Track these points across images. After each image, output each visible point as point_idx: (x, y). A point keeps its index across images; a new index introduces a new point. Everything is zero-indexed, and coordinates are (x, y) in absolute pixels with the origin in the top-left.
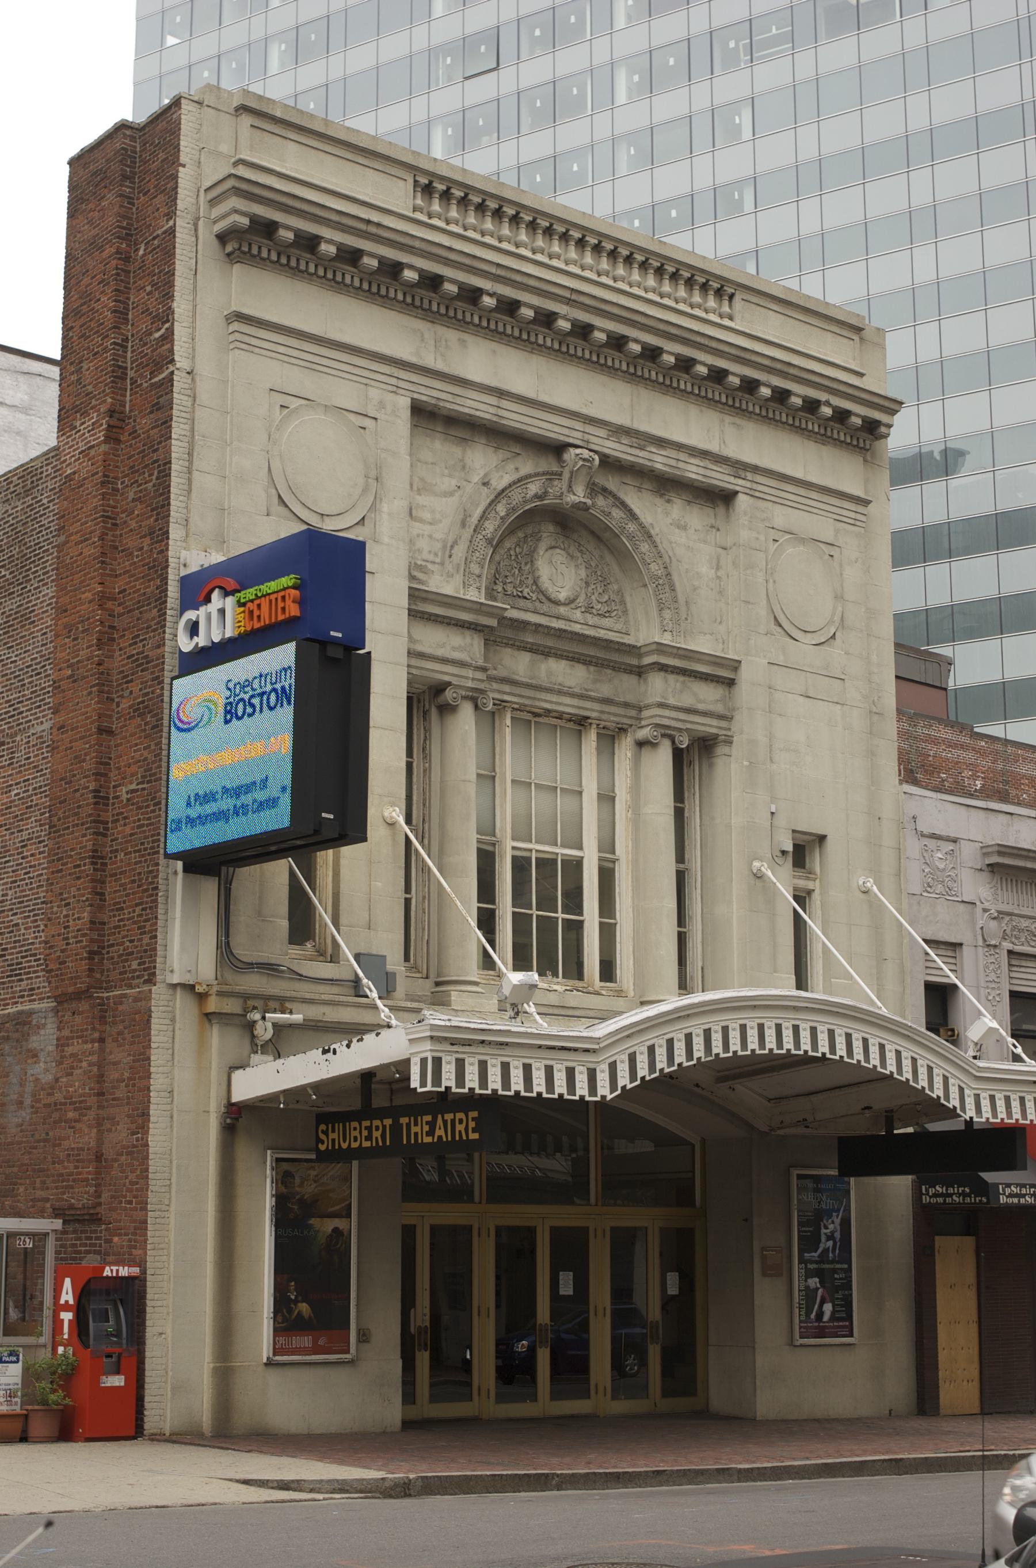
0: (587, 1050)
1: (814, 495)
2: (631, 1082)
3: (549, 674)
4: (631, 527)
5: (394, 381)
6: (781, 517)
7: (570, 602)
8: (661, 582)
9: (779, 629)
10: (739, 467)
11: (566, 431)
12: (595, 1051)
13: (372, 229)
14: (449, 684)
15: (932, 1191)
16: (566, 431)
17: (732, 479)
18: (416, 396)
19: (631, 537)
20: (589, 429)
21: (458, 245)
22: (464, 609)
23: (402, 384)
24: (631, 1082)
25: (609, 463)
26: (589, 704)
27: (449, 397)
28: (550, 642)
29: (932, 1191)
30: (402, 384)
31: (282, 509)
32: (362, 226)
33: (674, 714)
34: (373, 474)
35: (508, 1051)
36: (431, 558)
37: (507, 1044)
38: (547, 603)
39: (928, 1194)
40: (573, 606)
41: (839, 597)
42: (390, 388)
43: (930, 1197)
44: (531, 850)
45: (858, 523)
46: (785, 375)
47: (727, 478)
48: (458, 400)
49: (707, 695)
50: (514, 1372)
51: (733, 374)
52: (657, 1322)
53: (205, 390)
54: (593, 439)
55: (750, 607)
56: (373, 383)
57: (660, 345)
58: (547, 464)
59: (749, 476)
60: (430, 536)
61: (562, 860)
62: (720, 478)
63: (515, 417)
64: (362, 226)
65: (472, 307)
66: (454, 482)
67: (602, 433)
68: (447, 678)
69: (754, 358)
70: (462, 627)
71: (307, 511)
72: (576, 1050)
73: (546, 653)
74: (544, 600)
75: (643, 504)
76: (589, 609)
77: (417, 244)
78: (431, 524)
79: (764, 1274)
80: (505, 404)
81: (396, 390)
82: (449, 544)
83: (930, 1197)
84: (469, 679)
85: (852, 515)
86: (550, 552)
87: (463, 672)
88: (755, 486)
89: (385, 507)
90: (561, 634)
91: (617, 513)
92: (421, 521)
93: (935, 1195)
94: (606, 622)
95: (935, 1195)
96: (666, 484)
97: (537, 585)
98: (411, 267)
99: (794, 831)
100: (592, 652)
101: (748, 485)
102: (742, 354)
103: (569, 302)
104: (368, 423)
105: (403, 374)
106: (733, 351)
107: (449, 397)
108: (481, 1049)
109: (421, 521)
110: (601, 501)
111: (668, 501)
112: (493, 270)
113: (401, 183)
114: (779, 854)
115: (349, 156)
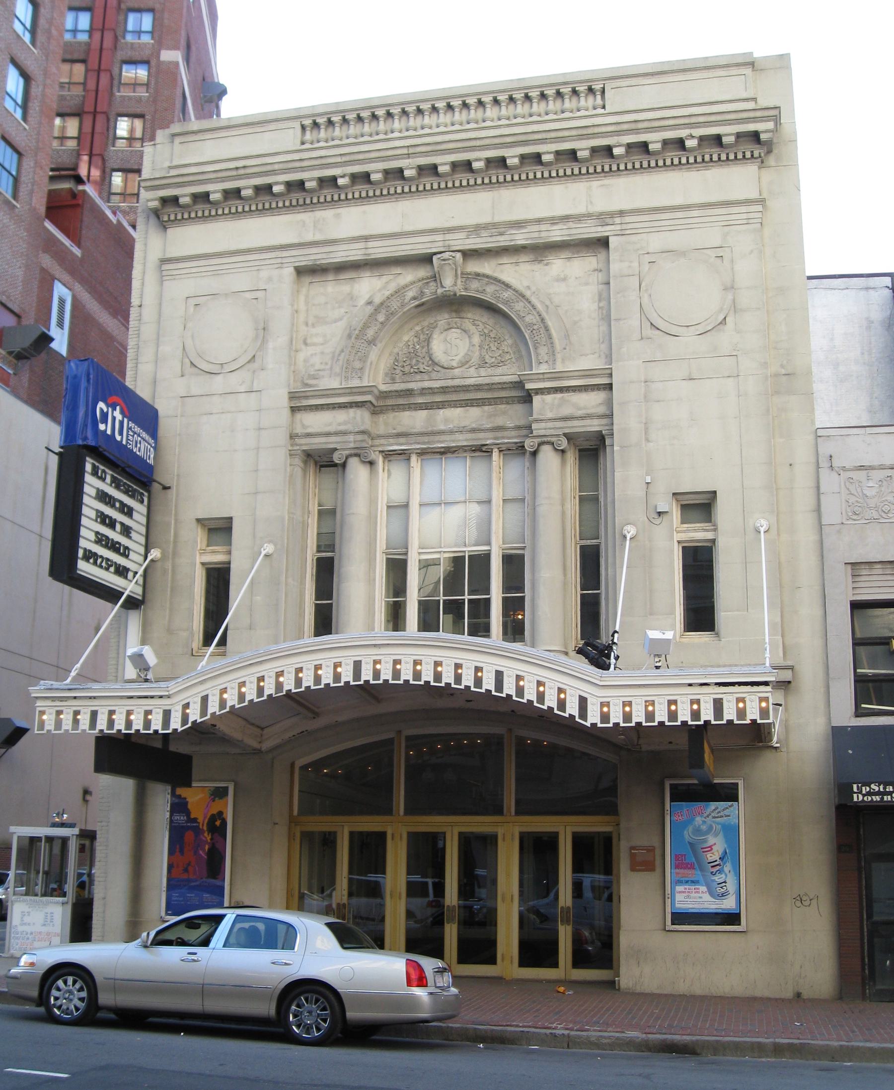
0: (161, 697)
1: (695, 213)
2: (201, 718)
3: (446, 421)
4: (507, 294)
5: (279, 261)
6: (656, 242)
7: (462, 364)
8: (535, 327)
9: (658, 332)
10: (603, 218)
11: (429, 245)
12: (169, 697)
13: (242, 172)
14: (336, 449)
15: (865, 790)
16: (429, 245)
17: (600, 229)
18: (297, 264)
19: (506, 302)
20: (448, 237)
21: (483, 134)
22: (340, 395)
23: (285, 260)
24: (201, 718)
25: (468, 254)
26: (481, 435)
27: (324, 256)
28: (438, 398)
29: (865, 790)
30: (285, 260)
31: (194, 370)
32: (234, 173)
33: (550, 425)
34: (261, 326)
35: (96, 702)
36: (322, 367)
37: (95, 698)
38: (443, 370)
39: (861, 792)
40: (467, 366)
41: (730, 288)
42: (276, 266)
43: (864, 795)
44: (464, 552)
45: (751, 221)
46: (636, 131)
47: (593, 229)
48: (332, 255)
49: (592, 401)
50: (537, 951)
51: (245, 188)
52: (569, 907)
53: (148, 314)
54: (452, 243)
55: (621, 322)
56: (263, 267)
57: (501, 155)
58: (422, 272)
59: (618, 220)
60: (322, 353)
61: (469, 556)
62: (592, 231)
63: (379, 250)
64: (234, 173)
65: (718, 149)
66: (343, 311)
67: (462, 235)
68: (332, 446)
69: (596, 130)
70: (345, 407)
71: (211, 365)
72: (152, 697)
73: (441, 405)
74: (439, 369)
75: (516, 274)
76: (483, 364)
77: (276, 167)
78: (322, 344)
79: (633, 869)
80: (370, 244)
81: (281, 266)
82: (337, 354)
83: (864, 795)
84: (351, 441)
85: (745, 216)
86: (445, 333)
87: (346, 438)
88: (624, 226)
89: (271, 345)
90: (444, 390)
91: (490, 289)
92: (314, 344)
93: (869, 794)
94: (499, 371)
95: (869, 794)
96: (541, 250)
97: (433, 361)
98: (277, 183)
99: (674, 494)
100: (479, 395)
101: (618, 227)
102: (585, 132)
103: (408, 156)
104: (259, 294)
105: (285, 254)
106: (574, 133)
107: (324, 256)
108: (75, 703)
109: (314, 344)
110: (475, 285)
111: (547, 265)
112: (339, 160)
113: (291, 131)
114: (656, 516)
115: (250, 131)
